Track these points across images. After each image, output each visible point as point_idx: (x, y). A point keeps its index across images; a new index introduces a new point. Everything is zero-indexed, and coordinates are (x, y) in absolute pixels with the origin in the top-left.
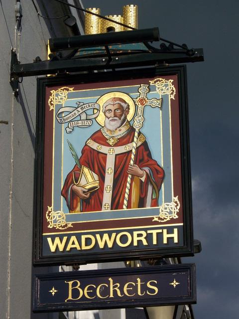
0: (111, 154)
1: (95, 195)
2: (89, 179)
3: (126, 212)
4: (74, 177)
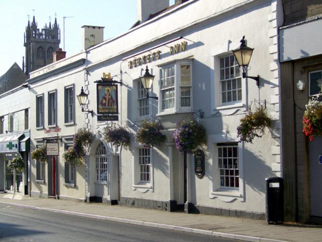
0: (107, 97)
1: (105, 104)
2: (104, 101)
3: (109, 107)
4: (102, 101)
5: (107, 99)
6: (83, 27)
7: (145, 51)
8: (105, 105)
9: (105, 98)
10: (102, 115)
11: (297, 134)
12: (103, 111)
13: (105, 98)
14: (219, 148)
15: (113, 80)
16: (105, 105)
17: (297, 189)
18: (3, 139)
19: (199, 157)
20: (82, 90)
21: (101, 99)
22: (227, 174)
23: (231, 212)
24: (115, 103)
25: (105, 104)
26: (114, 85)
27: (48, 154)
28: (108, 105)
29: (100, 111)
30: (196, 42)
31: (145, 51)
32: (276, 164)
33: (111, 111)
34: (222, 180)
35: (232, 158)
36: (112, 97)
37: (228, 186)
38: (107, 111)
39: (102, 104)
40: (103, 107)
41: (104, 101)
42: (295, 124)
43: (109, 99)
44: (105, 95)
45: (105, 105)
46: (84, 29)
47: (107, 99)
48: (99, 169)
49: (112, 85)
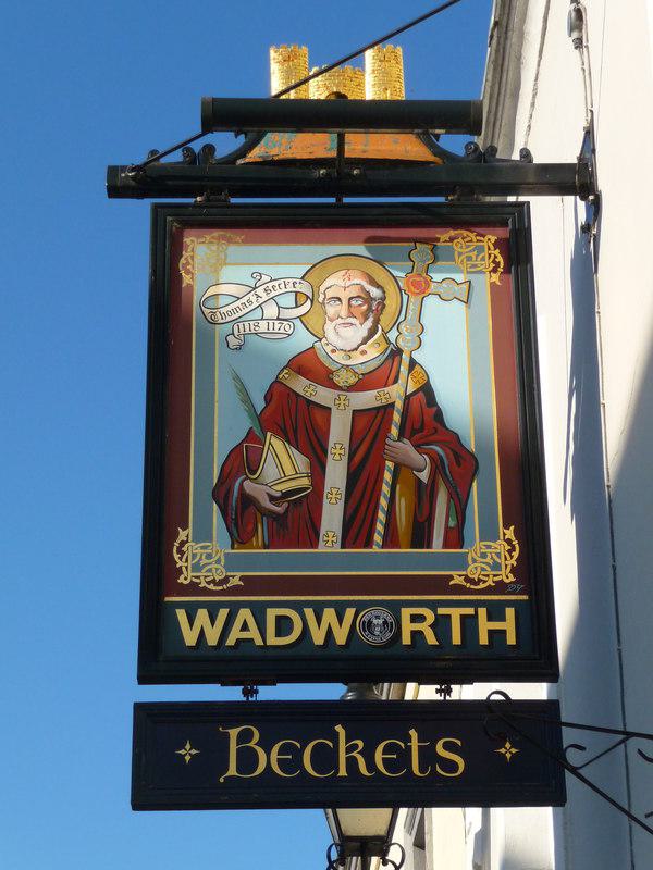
2: (282, 466)
3: (376, 559)
4: (245, 459)
5: (339, 432)
6: (119, 188)
8: (309, 534)
10: (334, 691)
12: (245, 631)
18: (256, 154)
23: (417, 368)
28: (356, 530)
30: (513, 698)
33: (415, 624)
38: (331, 627)
39: (241, 516)
41: (282, 466)
42: (622, 690)
43: (370, 425)
46: (139, 211)
47: (339, 432)
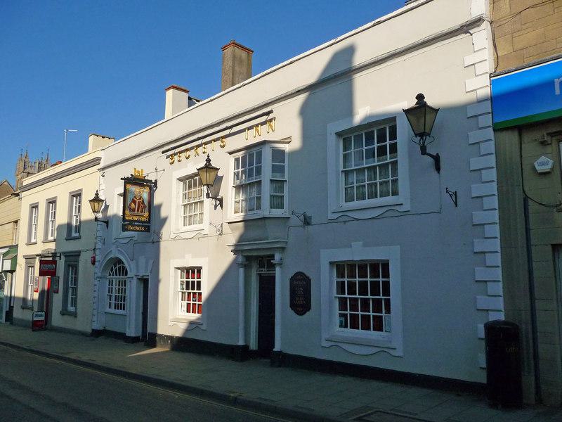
3: (139, 213)
7: (153, 125)
8: (135, 211)
9: (134, 202)
11: (533, 248)
13: (134, 202)
14: (200, 290)
15: (146, 178)
16: (134, 210)
17: (235, 402)
19: (300, 283)
20: (97, 194)
21: (129, 202)
22: (354, 308)
24: (147, 209)
25: (135, 209)
26: (147, 186)
27: (399, 246)
28: (138, 210)
29: (127, 218)
31: (153, 125)
32: (487, 297)
34: (343, 319)
35: (197, 303)
36: (143, 201)
37: (369, 329)
40: (132, 213)
41: (133, 206)
43: (139, 202)
44: (135, 197)
45: (134, 210)
48: (114, 294)
49: (143, 186)
